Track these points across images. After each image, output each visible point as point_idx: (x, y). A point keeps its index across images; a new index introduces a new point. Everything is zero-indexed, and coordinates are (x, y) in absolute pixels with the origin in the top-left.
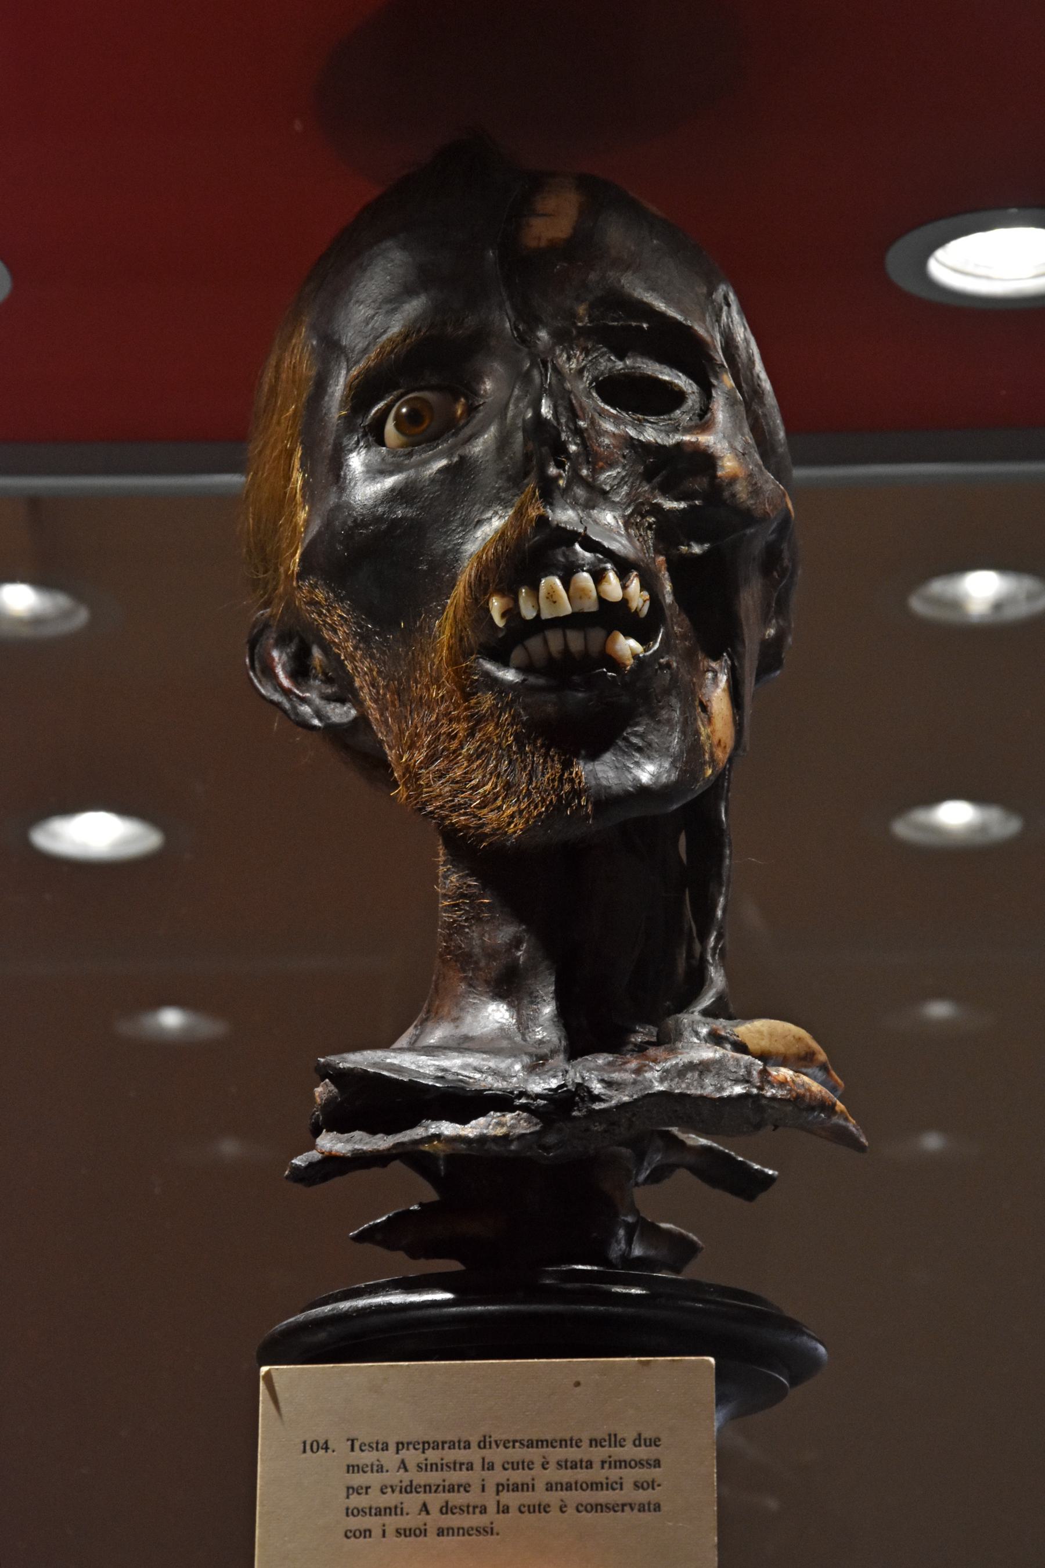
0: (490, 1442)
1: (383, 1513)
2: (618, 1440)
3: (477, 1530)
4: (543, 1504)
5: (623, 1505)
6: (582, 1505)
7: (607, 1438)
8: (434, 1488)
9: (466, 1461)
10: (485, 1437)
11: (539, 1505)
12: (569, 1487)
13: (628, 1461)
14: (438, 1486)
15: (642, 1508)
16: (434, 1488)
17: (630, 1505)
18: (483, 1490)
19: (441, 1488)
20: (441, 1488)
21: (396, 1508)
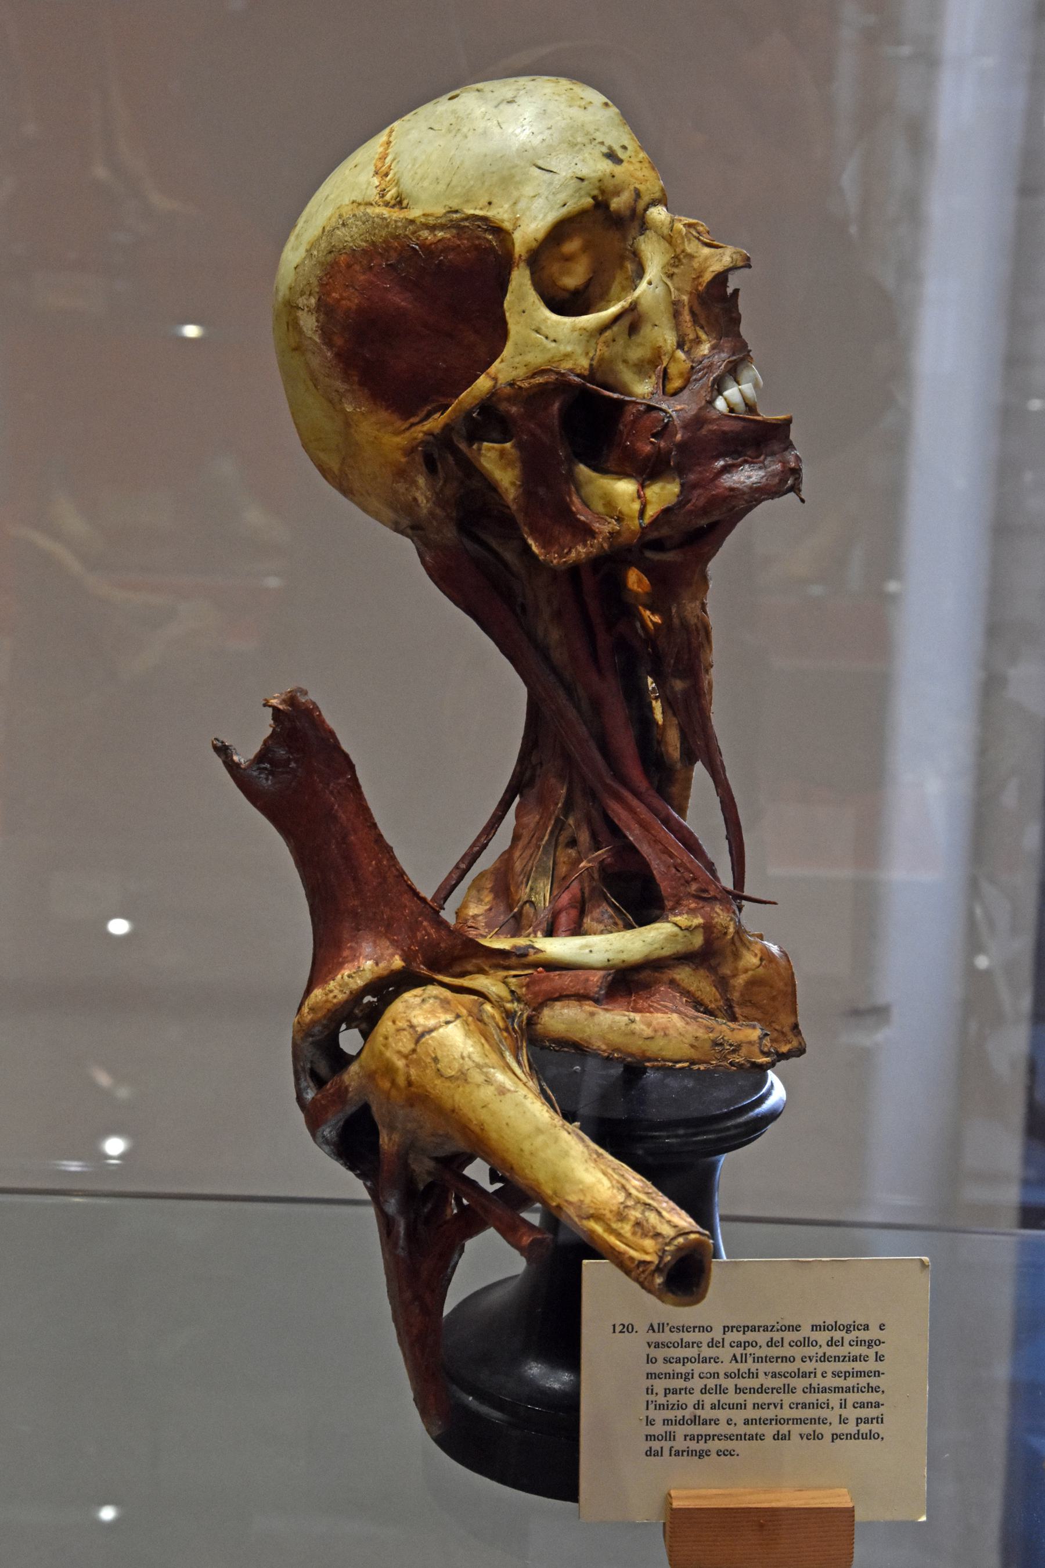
0: (858, 1388)
1: (807, 1407)
2: (707, 1389)
3: (725, 1437)
4: (822, 1418)
5: (769, 1404)
6: (727, 1451)
7: (714, 1388)
8: (841, 1359)
9: (689, 1434)
10: (699, 1401)
11: (819, 1419)
12: (848, 1390)
13: (788, 1357)
14: (845, 1357)
15: (751, 1438)
16: (841, 1359)
17: (809, 1357)
18: (775, 903)
19: (847, 1358)
20: (847, 1358)
21: (853, 1387)
